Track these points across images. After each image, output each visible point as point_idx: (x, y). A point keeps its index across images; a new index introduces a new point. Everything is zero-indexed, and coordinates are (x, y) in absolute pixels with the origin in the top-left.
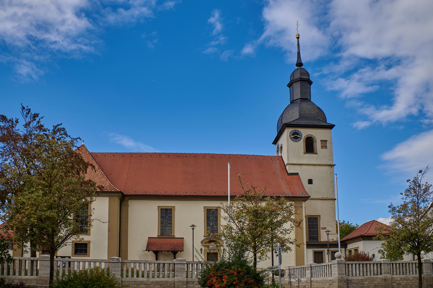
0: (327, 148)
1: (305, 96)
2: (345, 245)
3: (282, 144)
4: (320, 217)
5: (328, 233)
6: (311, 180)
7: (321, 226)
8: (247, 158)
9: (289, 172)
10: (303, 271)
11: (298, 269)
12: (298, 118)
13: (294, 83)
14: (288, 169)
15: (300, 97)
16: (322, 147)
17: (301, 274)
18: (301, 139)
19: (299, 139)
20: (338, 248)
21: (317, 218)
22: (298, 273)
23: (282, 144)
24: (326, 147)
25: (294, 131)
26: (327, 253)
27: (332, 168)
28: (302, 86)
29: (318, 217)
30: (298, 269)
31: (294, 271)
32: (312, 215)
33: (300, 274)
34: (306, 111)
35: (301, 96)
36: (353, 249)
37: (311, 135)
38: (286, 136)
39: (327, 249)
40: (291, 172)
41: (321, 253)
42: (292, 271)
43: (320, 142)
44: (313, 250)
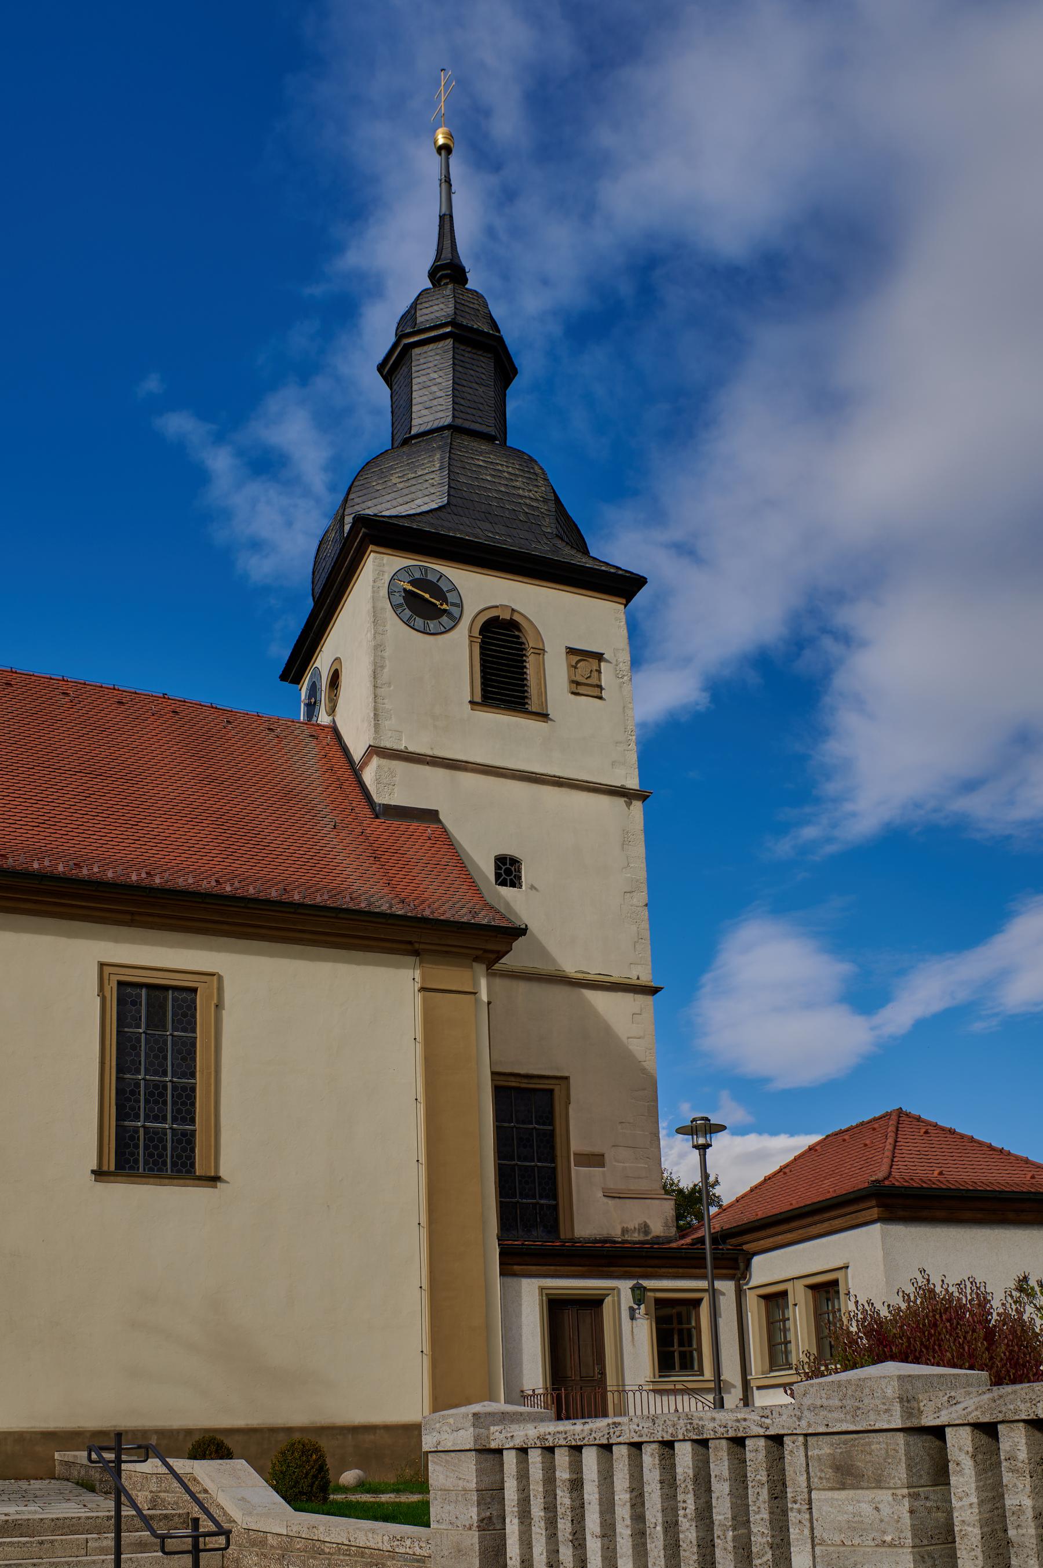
0: (600, 698)
1: (479, 420)
2: (736, 1260)
3: (337, 660)
4: (569, 1083)
5: (701, 1141)
6: (505, 880)
7: (576, 1146)
8: (120, 703)
9: (377, 799)
10: (721, 1489)
11: (621, 1453)
12: (440, 508)
13: (416, 351)
14: (378, 781)
15: (448, 421)
16: (577, 688)
17: (689, 1533)
18: (456, 621)
19: (444, 619)
20: (705, 1268)
21: (552, 1091)
22: (623, 1512)
23: (337, 660)
24: (597, 691)
25: (408, 612)
26: (632, 1310)
27: (632, 808)
28: (460, 369)
29: (557, 1089)
30: (621, 1453)
31: (563, 1474)
32: (522, 1071)
33: (671, 1527)
34: (489, 478)
35: (454, 417)
36: (800, 1285)
37: (513, 610)
38: (370, 594)
39: (631, 1283)
40: (393, 803)
41: (594, 1304)
42: (523, 1476)
43: (564, 655)
44: (542, 1289)
